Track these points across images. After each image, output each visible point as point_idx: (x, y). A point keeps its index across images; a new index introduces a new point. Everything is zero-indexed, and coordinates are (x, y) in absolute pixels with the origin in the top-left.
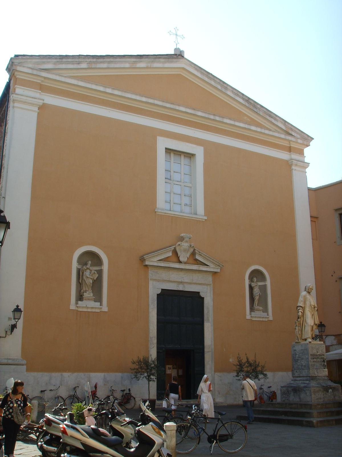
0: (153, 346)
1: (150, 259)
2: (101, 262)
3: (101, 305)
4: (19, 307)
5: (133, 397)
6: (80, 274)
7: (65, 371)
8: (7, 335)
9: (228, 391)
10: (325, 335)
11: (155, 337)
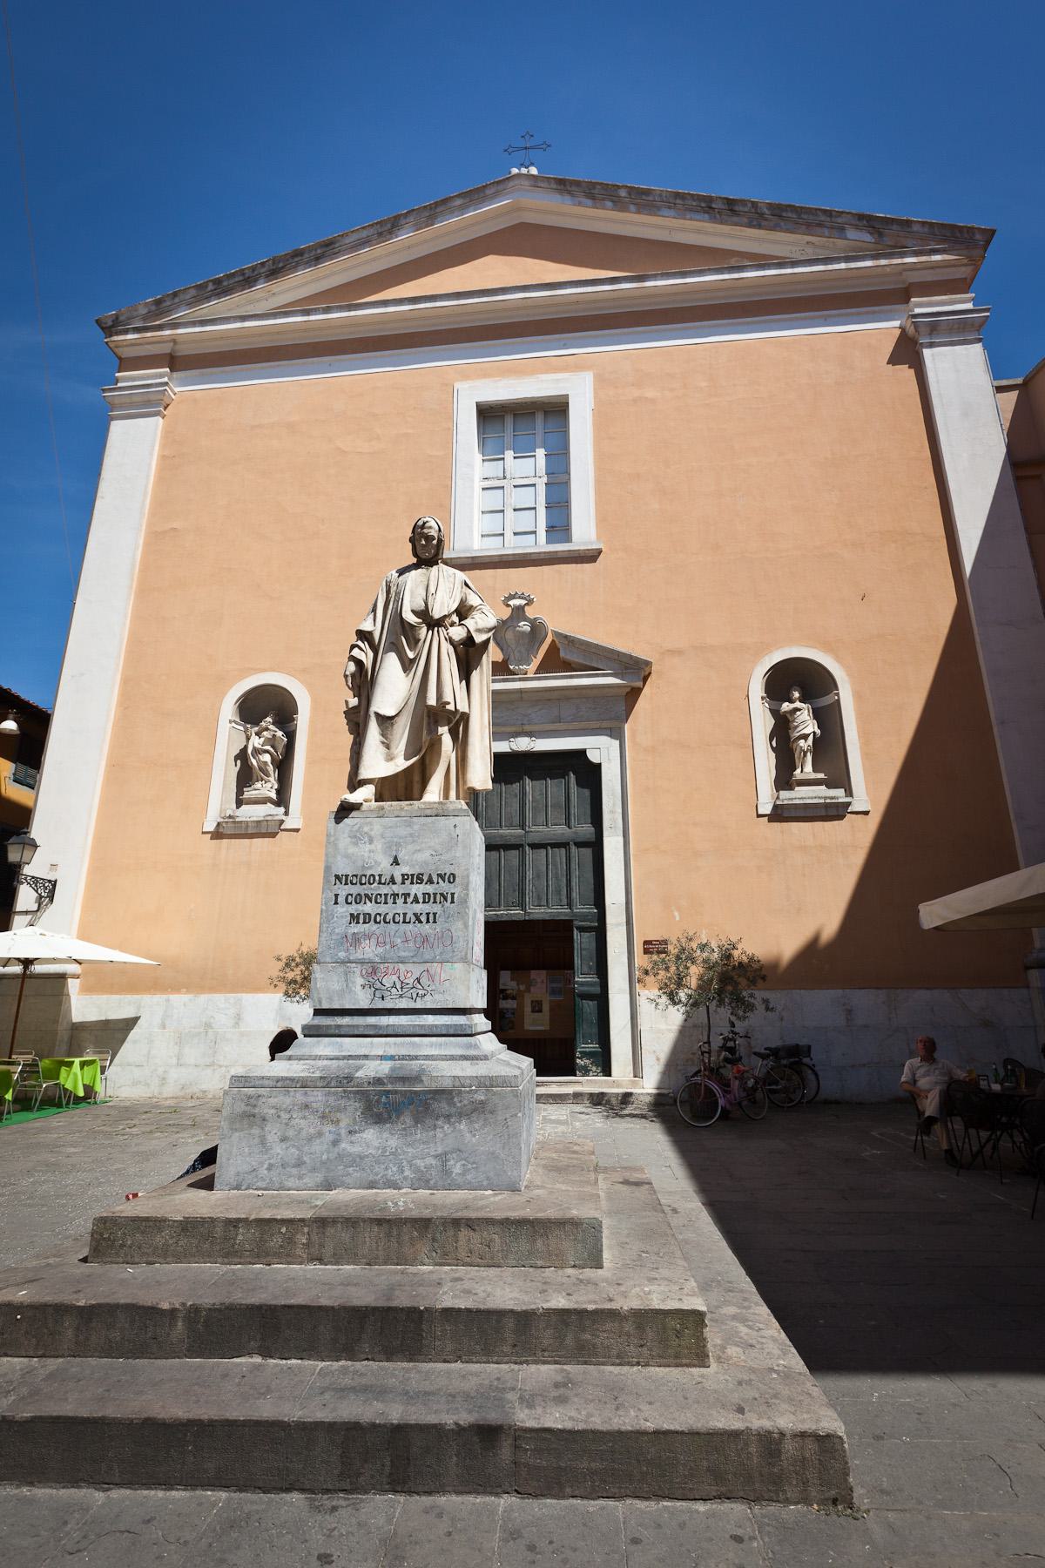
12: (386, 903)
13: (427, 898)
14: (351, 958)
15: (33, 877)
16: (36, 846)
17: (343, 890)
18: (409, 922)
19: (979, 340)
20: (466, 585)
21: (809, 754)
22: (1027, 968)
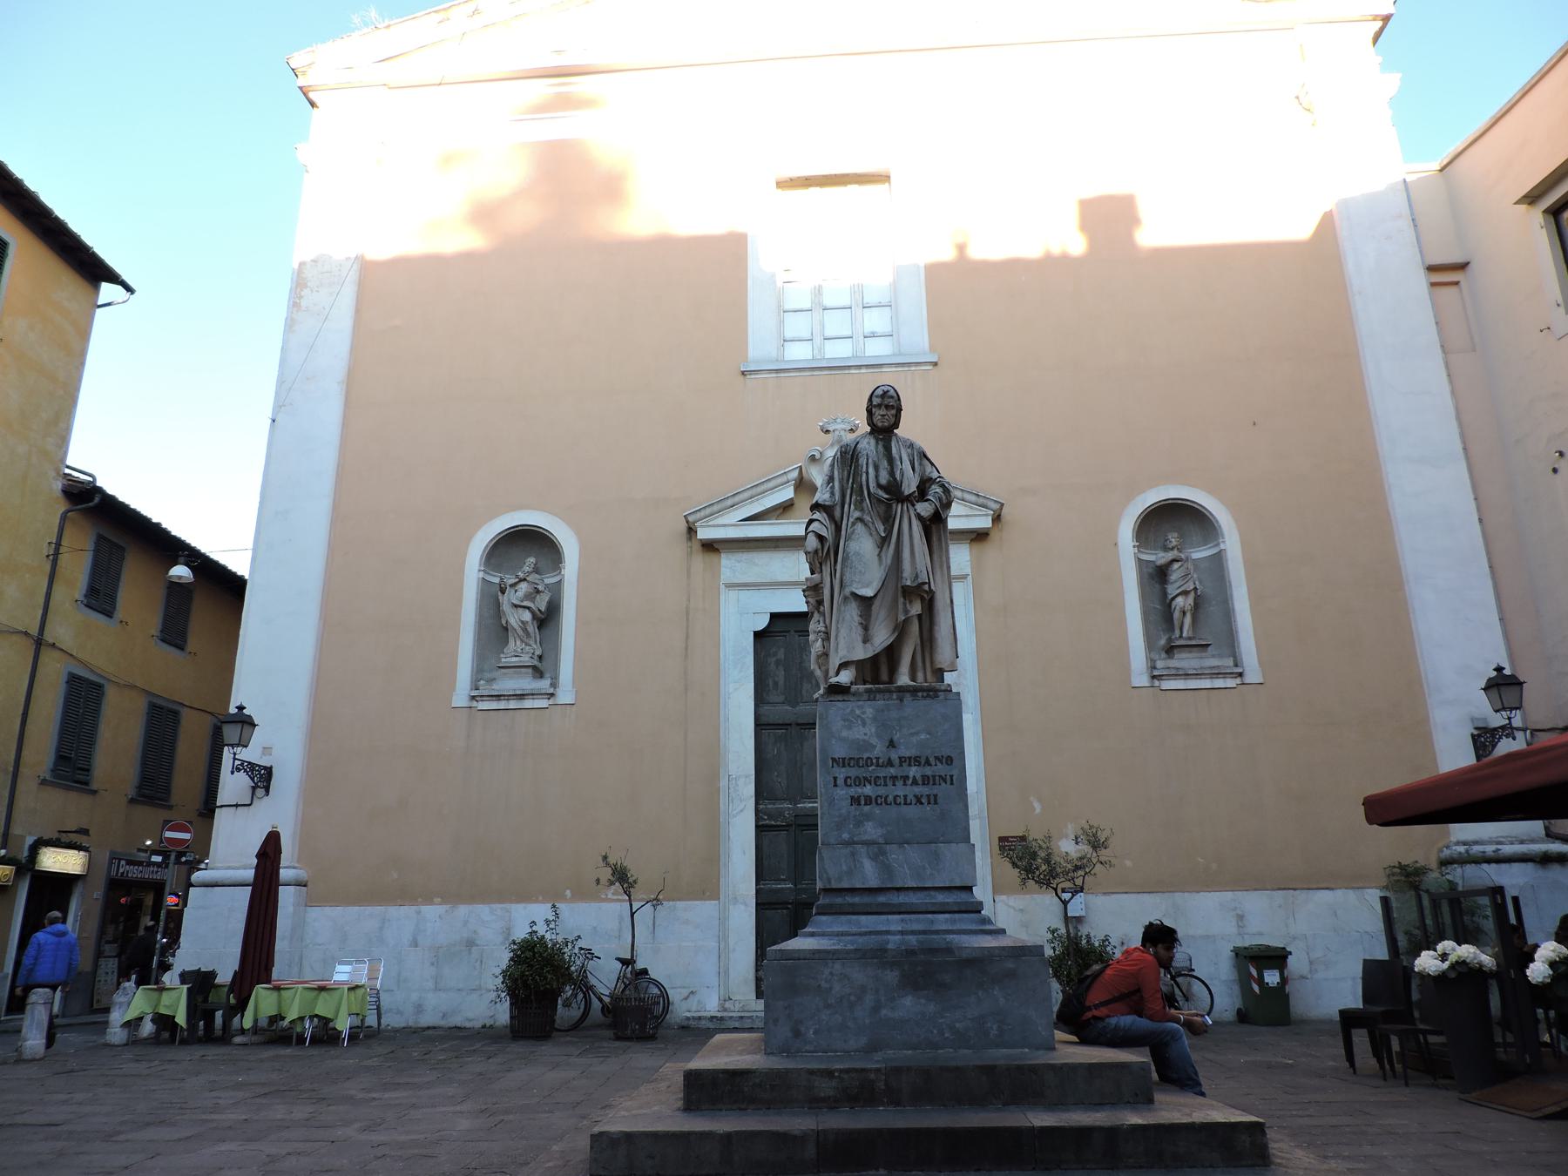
1: (715, 518)
2: (557, 546)
6: (491, 600)
7: (428, 900)
8: (255, 797)
12: (886, 785)
13: (926, 780)
14: (855, 839)
15: (249, 763)
17: (841, 773)
18: (911, 804)
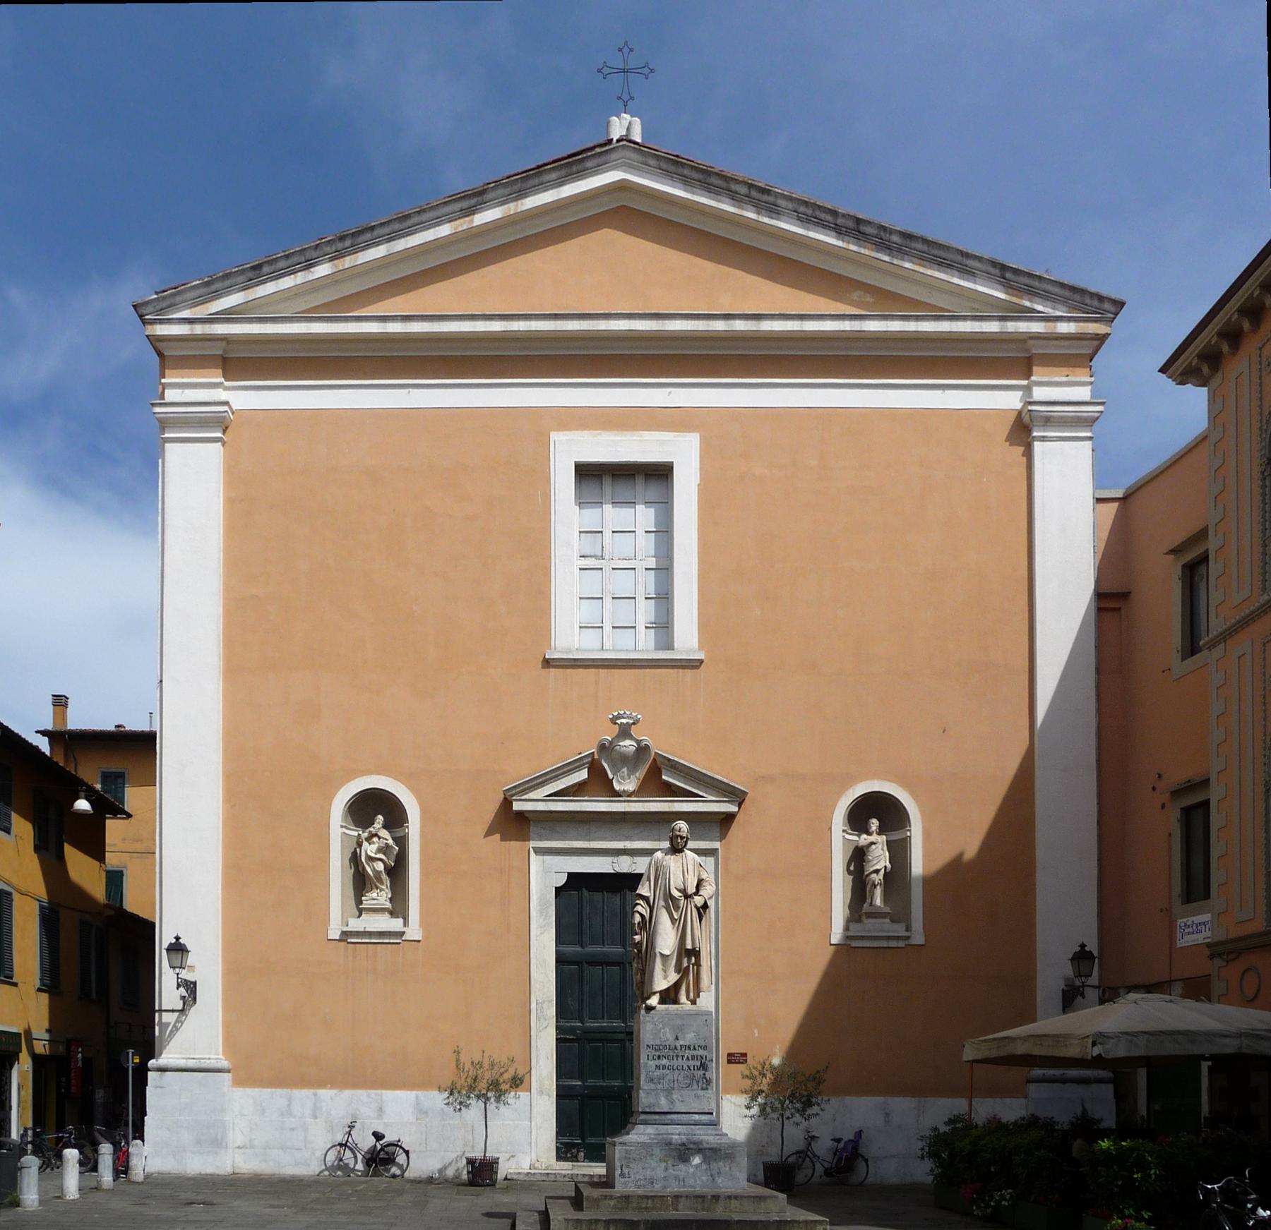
0: (546, 1024)
3: (405, 925)
4: (1087, 949)
5: (863, 1157)
7: (321, 1084)
9: (763, 1146)
10: (1126, 987)
11: (550, 1001)
15: (185, 980)
16: (188, 952)
19: (1090, 438)
20: (700, 865)
21: (878, 887)
22: (1028, 1082)
